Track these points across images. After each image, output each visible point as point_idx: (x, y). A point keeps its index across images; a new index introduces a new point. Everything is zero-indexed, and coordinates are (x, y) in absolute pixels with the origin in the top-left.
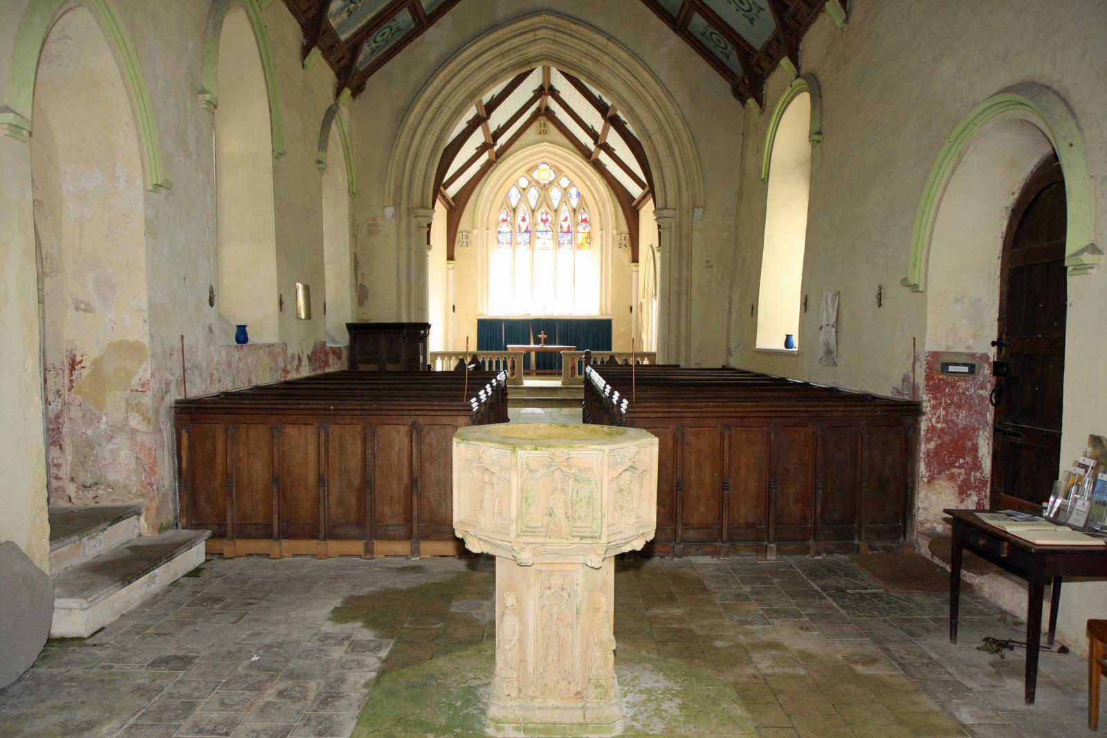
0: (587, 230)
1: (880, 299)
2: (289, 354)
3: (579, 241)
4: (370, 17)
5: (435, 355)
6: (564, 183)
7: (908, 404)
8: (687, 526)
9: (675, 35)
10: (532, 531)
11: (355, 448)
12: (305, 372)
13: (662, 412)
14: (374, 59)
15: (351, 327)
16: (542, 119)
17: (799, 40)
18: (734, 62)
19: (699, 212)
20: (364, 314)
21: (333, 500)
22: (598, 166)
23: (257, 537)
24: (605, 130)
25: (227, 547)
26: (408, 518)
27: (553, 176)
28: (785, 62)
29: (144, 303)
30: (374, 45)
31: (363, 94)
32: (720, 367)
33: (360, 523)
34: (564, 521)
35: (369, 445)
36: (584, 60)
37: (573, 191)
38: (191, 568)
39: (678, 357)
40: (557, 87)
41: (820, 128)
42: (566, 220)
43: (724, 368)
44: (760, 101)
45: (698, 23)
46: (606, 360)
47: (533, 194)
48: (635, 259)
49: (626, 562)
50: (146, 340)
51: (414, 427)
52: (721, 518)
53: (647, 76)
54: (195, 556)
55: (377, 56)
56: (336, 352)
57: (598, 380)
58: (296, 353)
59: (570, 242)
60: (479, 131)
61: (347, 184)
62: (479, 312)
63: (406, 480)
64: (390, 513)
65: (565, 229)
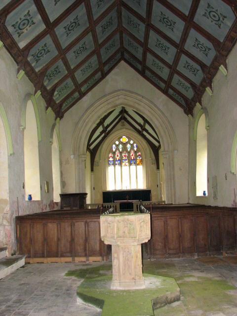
0: (141, 158)
1: (226, 178)
4: (66, 95)
5: (89, 205)
6: (132, 142)
7: (234, 208)
8: (170, 249)
10: (120, 237)
11: (68, 229)
12: (48, 210)
16: (123, 121)
17: (201, 97)
18: (183, 103)
19: (176, 152)
21: (62, 245)
23: (40, 257)
24: (144, 124)
25: (31, 261)
26: (85, 250)
28: (198, 104)
29: (8, 188)
31: (63, 119)
33: (71, 252)
34: (128, 234)
35: (73, 228)
37: (135, 145)
38: (22, 266)
39: (171, 201)
42: (133, 155)
44: (192, 115)
45: (171, 91)
47: (121, 146)
48: (158, 168)
49: (144, 246)
50: (8, 199)
51: (86, 222)
52: (180, 247)
54: (22, 262)
56: (57, 203)
59: (135, 163)
63: (84, 238)
64: (80, 249)
65: (133, 158)
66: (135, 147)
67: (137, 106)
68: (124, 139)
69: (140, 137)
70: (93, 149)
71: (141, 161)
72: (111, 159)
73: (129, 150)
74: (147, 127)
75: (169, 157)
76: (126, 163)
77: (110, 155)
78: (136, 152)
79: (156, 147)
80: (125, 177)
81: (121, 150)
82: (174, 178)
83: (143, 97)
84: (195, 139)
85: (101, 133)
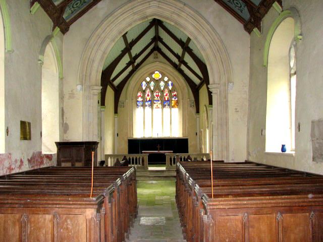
0: (177, 99)
2: (13, 160)
3: (173, 105)
9: (216, 3)
12: (26, 167)
13: (233, 204)
14: (73, 16)
15: (58, 144)
16: (156, 52)
20: (67, 137)
22: (181, 72)
27: (161, 76)
30: (72, 9)
31: (68, 33)
32: (244, 161)
36: (173, 15)
37: (170, 83)
40: (162, 37)
41: (301, 32)
42: (167, 95)
43: (247, 162)
46: (186, 157)
48: (198, 111)
53: (202, 21)
55: (75, 15)
56: (49, 157)
57: (182, 169)
58: (19, 159)
59: (169, 105)
60: (127, 55)
61: (58, 74)
62: (129, 136)
65: (166, 99)
66: (170, 85)
67: (175, 17)
68: (157, 75)
69: (176, 73)
70: (119, 86)
71: (177, 103)
72: (140, 99)
73: (162, 88)
74: (188, 58)
75: (220, 92)
76: (158, 104)
77: (139, 94)
78: (170, 92)
79: (196, 85)
80: (157, 121)
81: (152, 88)
82: (227, 123)
83: (185, 5)
84: (265, 64)
85: (128, 65)
